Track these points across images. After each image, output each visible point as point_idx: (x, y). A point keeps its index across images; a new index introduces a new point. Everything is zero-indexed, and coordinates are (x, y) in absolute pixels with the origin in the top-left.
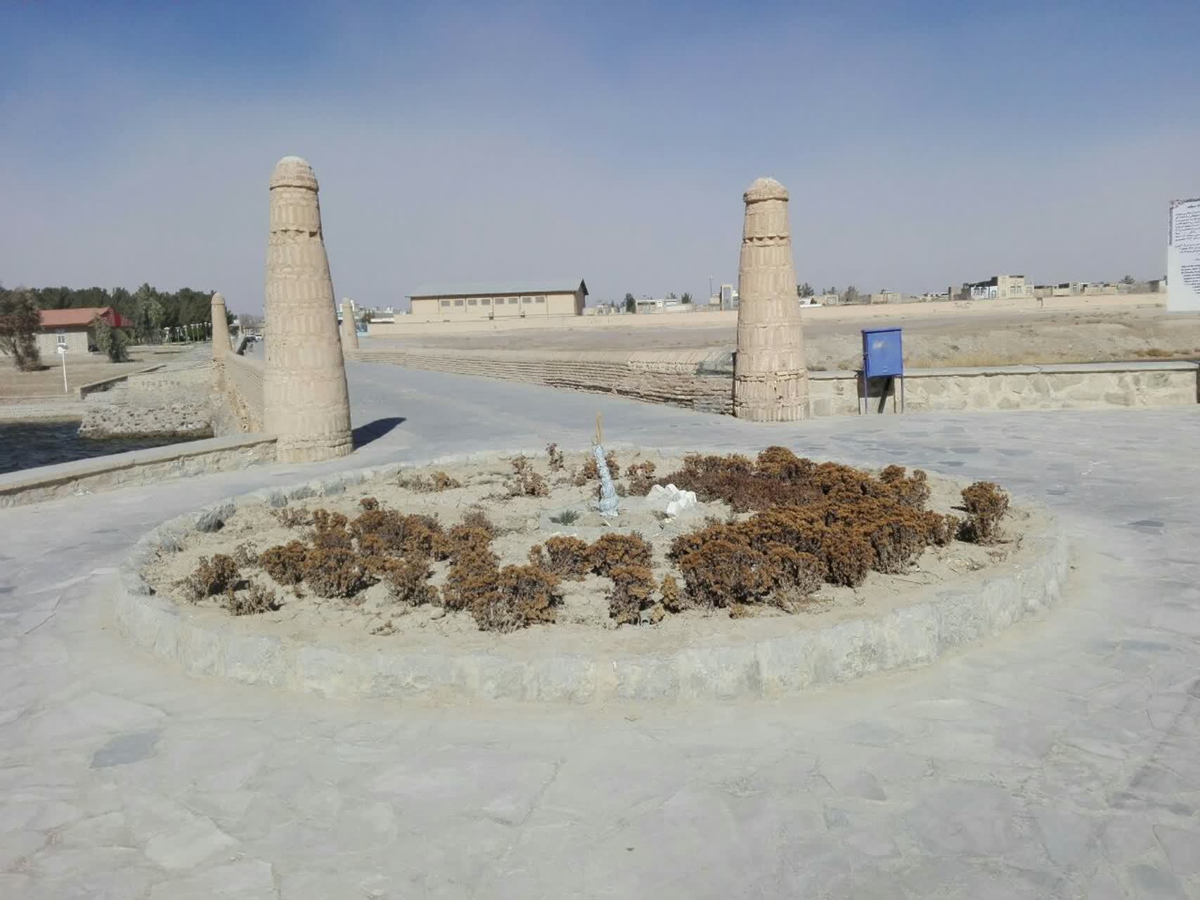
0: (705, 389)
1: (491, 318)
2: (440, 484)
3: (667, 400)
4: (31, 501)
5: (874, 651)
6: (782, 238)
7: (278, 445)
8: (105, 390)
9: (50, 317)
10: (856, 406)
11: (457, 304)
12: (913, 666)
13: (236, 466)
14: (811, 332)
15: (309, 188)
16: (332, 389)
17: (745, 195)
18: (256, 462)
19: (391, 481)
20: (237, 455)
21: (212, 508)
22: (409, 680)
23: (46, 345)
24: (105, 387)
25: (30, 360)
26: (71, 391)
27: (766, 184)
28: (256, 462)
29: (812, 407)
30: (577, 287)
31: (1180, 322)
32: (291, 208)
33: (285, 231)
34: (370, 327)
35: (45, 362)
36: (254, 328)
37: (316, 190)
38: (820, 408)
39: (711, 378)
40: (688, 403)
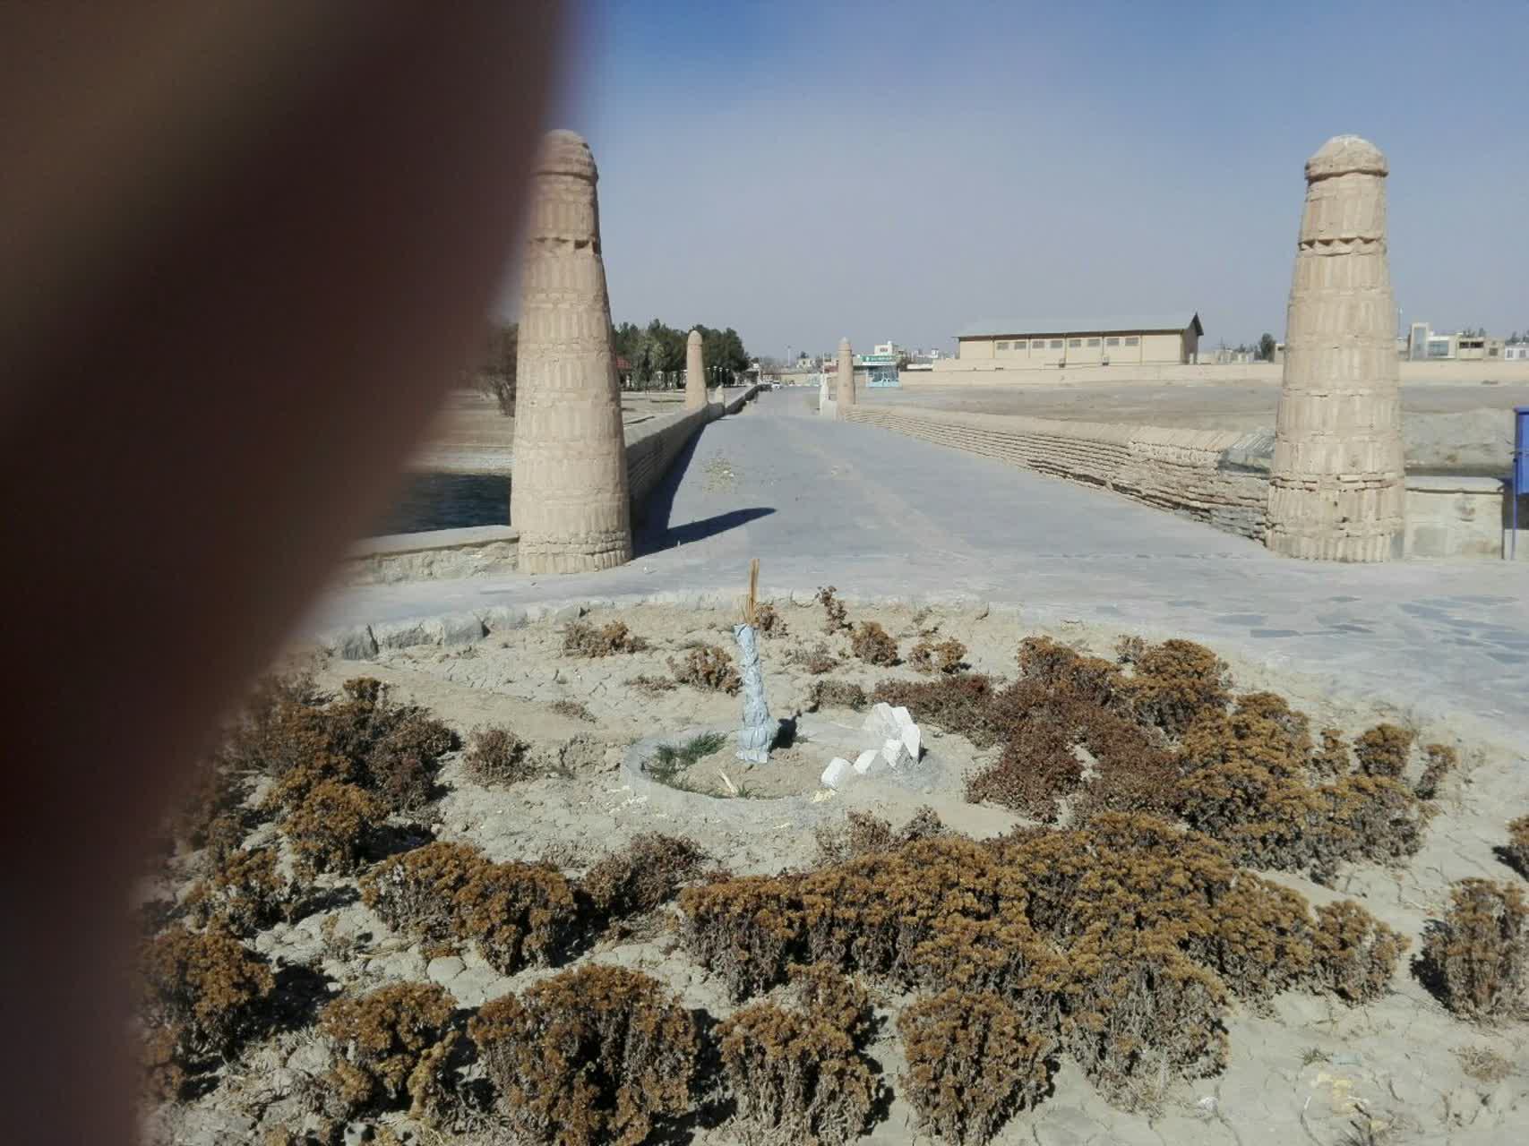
3: (1177, 505)
6: (1367, 241)
7: (521, 546)
10: (1497, 542)
11: (1036, 346)
13: (457, 573)
14: (1414, 403)
17: (1307, 168)
18: (486, 569)
20: (459, 557)
28: (486, 569)
30: (1185, 324)
34: (902, 374)
37: (593, 179)
38: (1427, 542)
40: (1203, 514)
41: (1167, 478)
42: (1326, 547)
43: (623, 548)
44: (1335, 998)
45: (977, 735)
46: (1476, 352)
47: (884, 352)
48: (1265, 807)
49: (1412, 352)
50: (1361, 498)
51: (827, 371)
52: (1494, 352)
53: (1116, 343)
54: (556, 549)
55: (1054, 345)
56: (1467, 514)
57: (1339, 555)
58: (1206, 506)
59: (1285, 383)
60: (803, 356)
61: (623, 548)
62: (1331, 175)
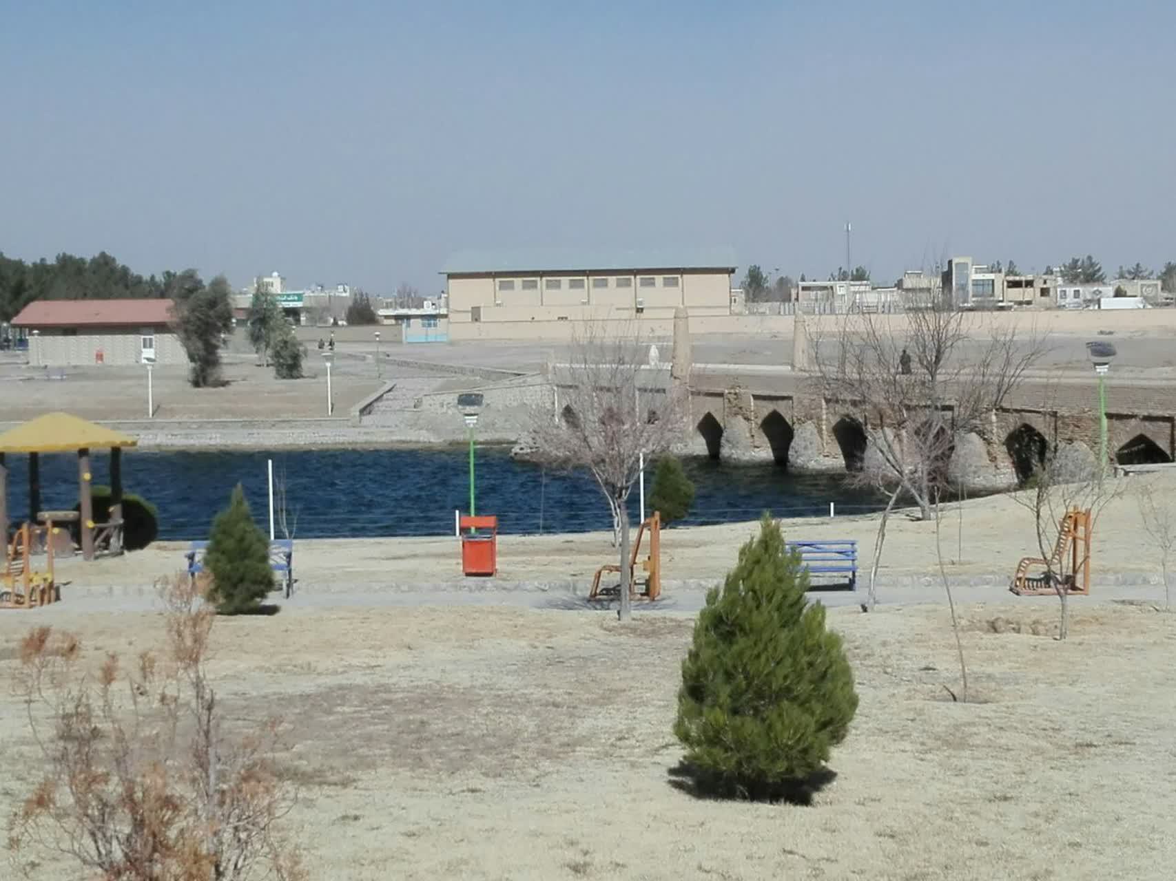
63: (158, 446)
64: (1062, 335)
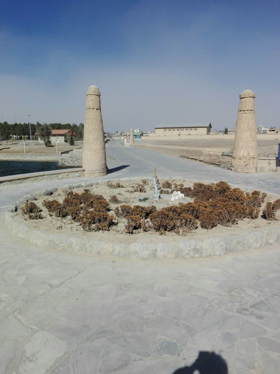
0: (224, 161)
1: (179, 135)
2: (117, 186)
4: (16, 184)
5: (198, 250)
6: (252, 111)
7: (85, 172)
8: (67, 153)
9: (54, 132)
10: (275, 169)
11: (173, 130)
12: (213, 257)
13: (73, 177)
14: (261, 144)
15: (97, 95)
16: (100, 156)
17: (240, 96)
18: (79, 176)
19: (105, 185)
20: (73, 174)
21: (50, 189)
22: (58, 243)
23: (53, 139)
24: (67, 152)
25: (48, 144)
26: (58, 153)
27: (248, 92)
28: (79, 176)
29: (259, 169)
30: (208, 125)
31: (61, 149)
32: (91, 101)
33: (90, 108)
34: (142, 137)
35: (52, 144)
36: (111, 137)
37: (99, 96)
38: (262, 169)
39: (226, 157)
40: (219, 165)
41: (211, 158)
42: (243, 170)
43: (106, 172)
44: (251, 219)
45: (191, 196)
46: (273, 132)
47: (137, 131)
48: (240, 199)
49: (259, 131)
50: (250, 161)
51: (124, 136)
52: (277, 132)
53: (192, 130)
54: (93, 172)
55: (178, 130)
56: (270, 164)
57: (246, 172)
58: (219, 163)
59: (235, 138)
60: (117, 132)
61: (106, 172)
62: (245, 98)
63: (18, 159)
64: (266, 140)
